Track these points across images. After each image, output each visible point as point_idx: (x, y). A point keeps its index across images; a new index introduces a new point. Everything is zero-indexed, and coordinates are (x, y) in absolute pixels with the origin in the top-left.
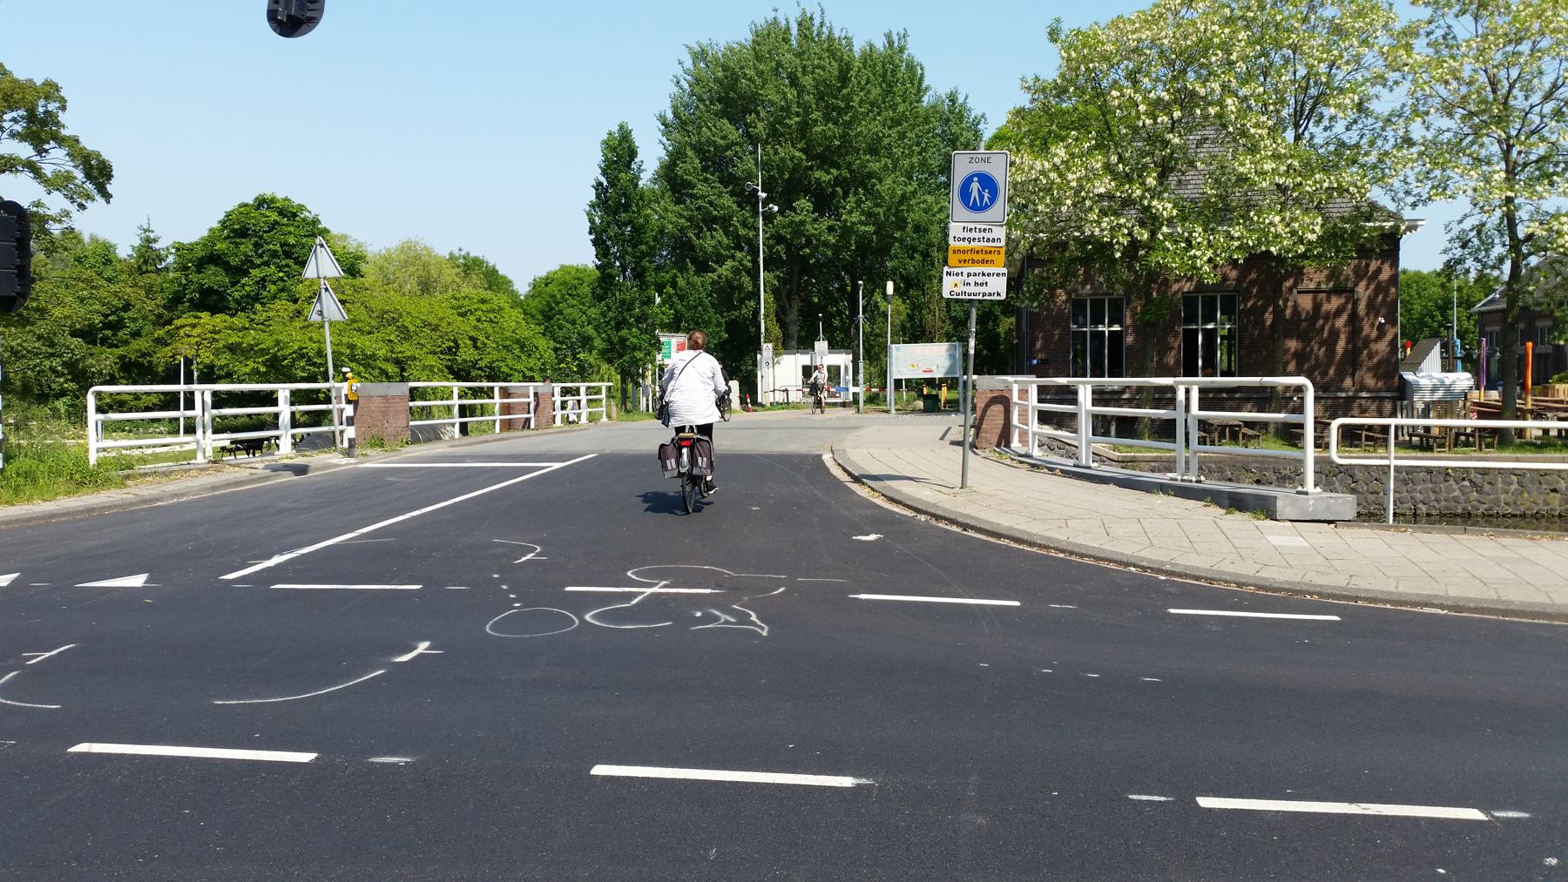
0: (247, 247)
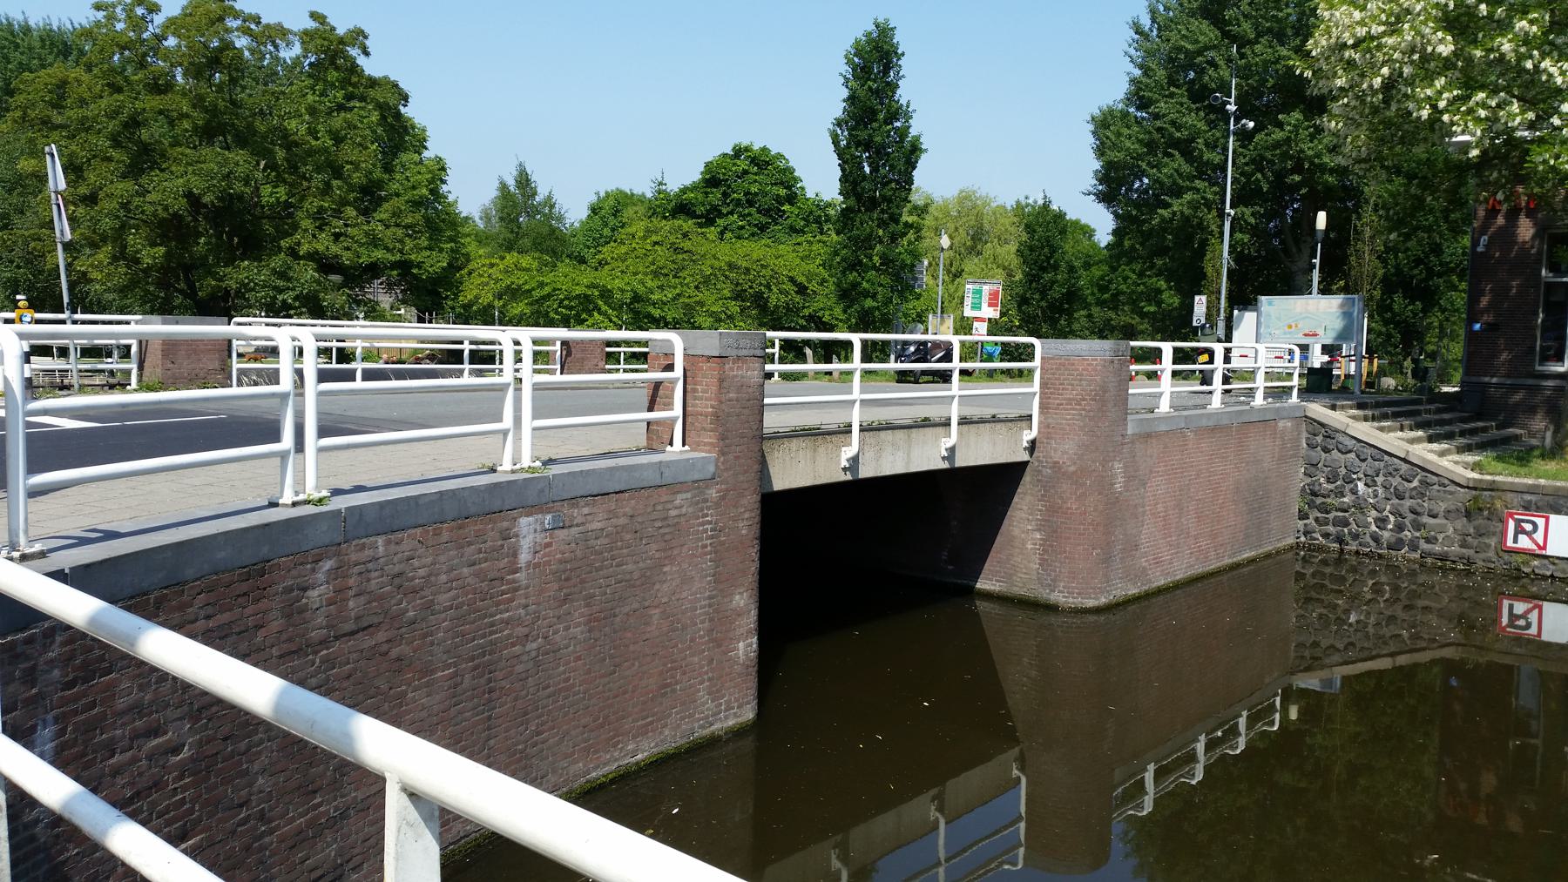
0: (716, 196)
